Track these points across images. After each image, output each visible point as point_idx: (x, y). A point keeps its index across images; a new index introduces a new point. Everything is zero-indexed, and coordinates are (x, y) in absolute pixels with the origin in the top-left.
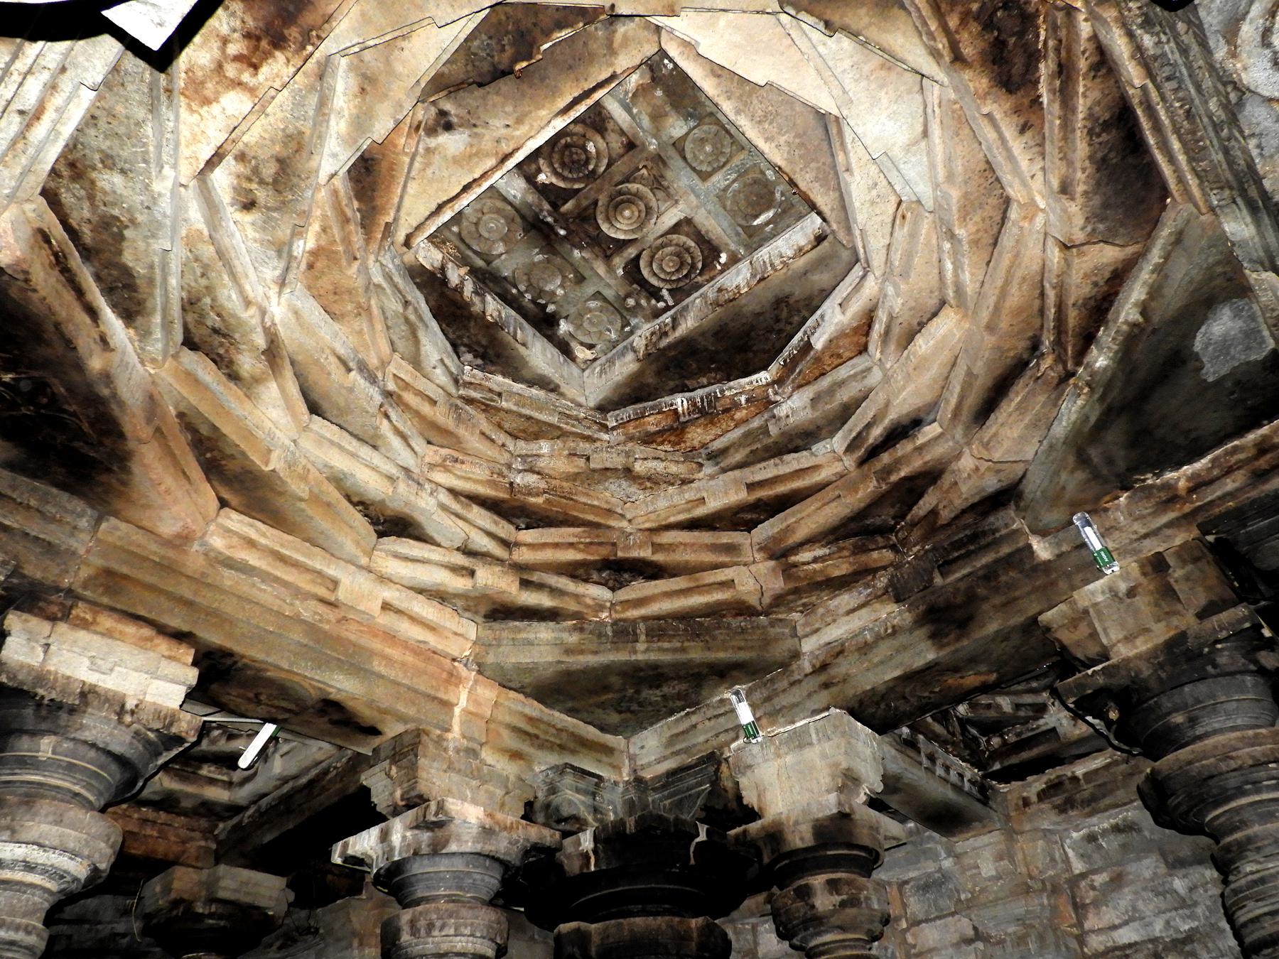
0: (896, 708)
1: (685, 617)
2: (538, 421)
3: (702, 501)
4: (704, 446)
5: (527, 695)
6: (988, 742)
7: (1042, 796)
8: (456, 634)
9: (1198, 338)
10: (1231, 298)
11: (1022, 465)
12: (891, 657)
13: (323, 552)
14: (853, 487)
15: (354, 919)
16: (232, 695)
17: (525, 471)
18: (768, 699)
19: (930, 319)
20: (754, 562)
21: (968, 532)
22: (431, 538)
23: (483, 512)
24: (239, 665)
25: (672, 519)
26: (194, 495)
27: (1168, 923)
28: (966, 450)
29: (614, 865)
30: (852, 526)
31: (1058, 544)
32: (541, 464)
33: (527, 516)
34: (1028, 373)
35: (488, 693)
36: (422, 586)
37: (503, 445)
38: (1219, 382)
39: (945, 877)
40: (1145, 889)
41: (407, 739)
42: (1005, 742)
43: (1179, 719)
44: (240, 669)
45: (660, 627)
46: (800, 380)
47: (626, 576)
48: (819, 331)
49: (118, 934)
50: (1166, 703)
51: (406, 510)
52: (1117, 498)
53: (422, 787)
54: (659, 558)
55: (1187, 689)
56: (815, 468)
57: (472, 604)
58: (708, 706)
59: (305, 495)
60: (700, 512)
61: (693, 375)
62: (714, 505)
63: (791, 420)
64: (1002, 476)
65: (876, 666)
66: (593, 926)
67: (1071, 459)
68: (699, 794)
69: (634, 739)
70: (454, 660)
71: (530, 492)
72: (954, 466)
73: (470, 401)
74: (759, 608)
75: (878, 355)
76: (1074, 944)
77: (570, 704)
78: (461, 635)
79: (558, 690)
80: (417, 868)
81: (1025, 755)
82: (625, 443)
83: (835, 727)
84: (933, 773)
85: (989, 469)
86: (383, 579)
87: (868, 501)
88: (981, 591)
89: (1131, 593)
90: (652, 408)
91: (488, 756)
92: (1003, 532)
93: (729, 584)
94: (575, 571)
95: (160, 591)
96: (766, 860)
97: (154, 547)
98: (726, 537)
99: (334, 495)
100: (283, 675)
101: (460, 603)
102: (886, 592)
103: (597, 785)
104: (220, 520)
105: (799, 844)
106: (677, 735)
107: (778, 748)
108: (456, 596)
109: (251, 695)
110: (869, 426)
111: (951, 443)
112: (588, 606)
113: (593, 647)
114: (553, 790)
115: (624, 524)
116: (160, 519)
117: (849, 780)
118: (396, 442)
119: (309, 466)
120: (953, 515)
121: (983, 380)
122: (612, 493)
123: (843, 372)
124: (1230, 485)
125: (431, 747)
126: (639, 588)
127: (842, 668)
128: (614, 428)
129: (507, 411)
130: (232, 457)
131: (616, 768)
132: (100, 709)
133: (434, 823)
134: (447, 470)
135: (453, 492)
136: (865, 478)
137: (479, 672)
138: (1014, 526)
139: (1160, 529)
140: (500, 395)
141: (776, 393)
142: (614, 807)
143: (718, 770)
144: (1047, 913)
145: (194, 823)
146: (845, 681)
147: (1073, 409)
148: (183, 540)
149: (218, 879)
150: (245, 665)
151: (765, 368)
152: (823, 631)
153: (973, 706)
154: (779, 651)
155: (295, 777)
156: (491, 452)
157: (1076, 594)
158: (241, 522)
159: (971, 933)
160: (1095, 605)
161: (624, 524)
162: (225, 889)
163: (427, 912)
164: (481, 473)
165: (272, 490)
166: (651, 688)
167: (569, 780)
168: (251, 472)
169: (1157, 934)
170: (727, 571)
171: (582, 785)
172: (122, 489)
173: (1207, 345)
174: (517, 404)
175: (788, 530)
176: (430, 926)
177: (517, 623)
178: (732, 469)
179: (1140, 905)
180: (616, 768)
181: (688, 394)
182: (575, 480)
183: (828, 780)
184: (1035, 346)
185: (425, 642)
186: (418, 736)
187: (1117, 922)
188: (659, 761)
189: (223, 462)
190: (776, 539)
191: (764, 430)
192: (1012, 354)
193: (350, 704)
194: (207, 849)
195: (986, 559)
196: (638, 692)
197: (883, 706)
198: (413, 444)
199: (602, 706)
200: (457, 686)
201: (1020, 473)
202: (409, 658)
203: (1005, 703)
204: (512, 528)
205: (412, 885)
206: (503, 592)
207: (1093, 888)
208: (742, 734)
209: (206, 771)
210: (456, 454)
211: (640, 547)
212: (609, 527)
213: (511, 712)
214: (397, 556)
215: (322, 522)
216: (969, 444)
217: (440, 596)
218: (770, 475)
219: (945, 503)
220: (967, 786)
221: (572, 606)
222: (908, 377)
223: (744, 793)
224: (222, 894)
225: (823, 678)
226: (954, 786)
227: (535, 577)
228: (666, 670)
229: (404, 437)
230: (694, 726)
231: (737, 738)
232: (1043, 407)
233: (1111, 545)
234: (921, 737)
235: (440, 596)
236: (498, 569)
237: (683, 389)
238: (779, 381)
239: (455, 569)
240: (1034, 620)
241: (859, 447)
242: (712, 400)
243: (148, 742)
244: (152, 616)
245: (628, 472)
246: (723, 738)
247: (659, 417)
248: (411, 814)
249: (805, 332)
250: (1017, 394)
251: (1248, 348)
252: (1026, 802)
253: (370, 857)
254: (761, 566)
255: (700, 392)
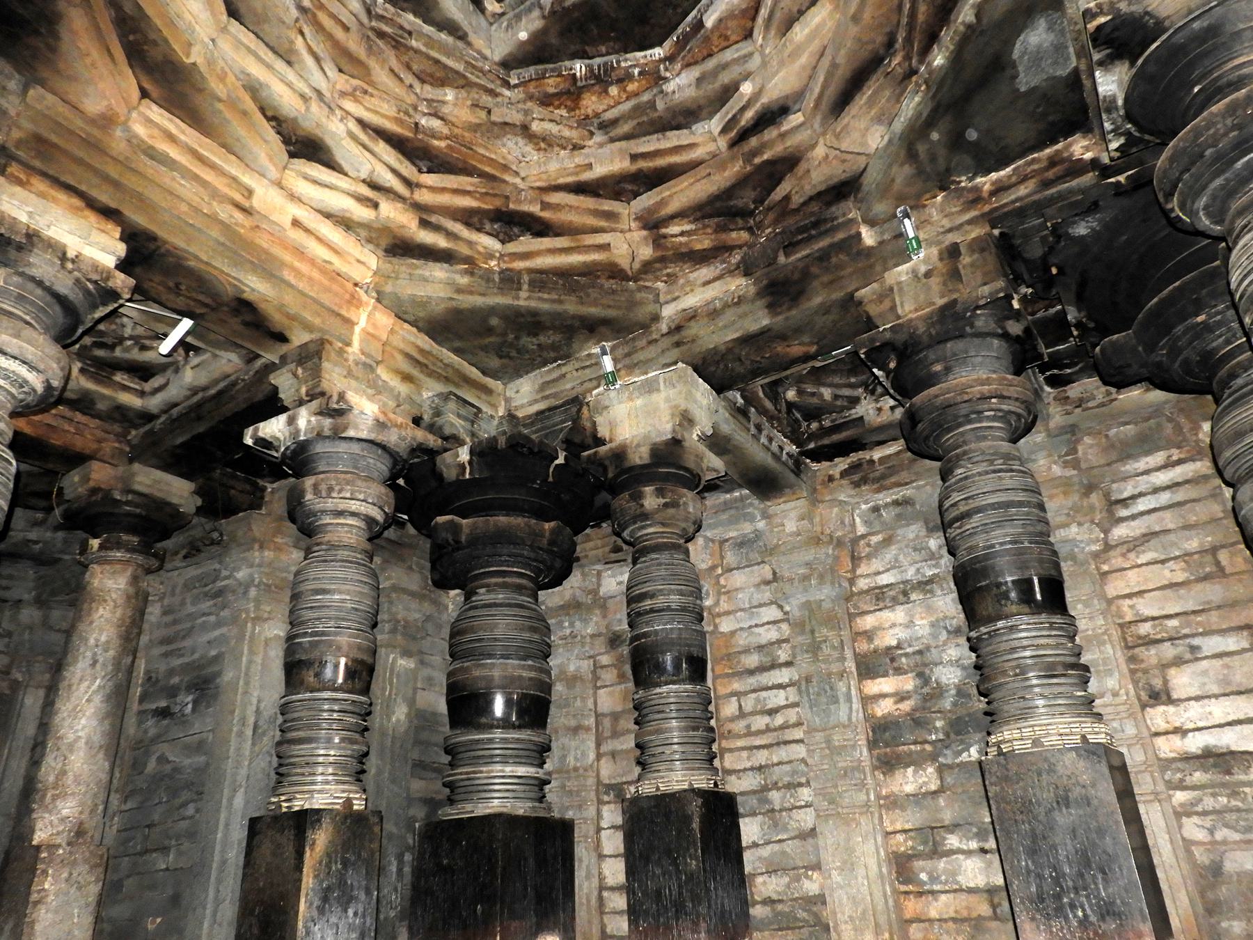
0: (733, 370)
1: (564, 274)
2: (445, 67)
3: (590, 166)
4: (597, 115)
5: (419, 330)
6: (808, 426)
7: (844, 474)
8: (358, 261)
9: (1017, 46)
10: (1047, 9)
11: (864, 158)
12: (734, 322)
13: (238, 161)
14: (722, 166)
15: (254, 527)
16: (155, 283)
17: (430, 114)
18: (628, 355)
19: (809, 8)
20: (630, 230)
21: (813, 219)
22: (340, 166)
23: (388, 148)
24: (163, 250)
25: (561, 181)
26: (118, 77)
27: (918, 569)
28: (821, 141)
29: (486, 474)
30: (718, 204)
31: (882, 233)
32: (446, 110)
33: (430, 160)
34: (881, 70)
35: (385, 320)
36: (329, 210)
37: (411, 86)
38: (1032, 91)
39: (758, 535)
40: (907, 546)
41: (312, 347)
42: (821, 427)
43: (938, 368)
44: (163, 255)
45: (541, 280)
46: (689, 59)
47: (516, 230)
48: (711, 9)
49: (29, 541)
50: (932, 356)
51: (318, 132)
52: (935, 197)
53: (325, 385)
54: (546, 215)
55: (949, 345)
56: (692, 146)
57: (374, 235)
58: (577, 359)
59: (223, 95)
60: (587, 176)
61: (594, 42)
62: (599, 171)
63: (677, 96)
64: (846, 166)
65: (721, 329)
66: (464, 521)
67: (903, 153)
68: (562, 430)
69: (511, 385)
70: (356, 285)
71: (434, 135)
72: (809, 155)
73: (381, 35)
74: (630, 273)
75: (760, 41)
76: (846, 584)
77: (457, 344)
78: (363, 263)
79: (448, 327)
80: (319, 448)
81: (836, 438)
82: (524, 102)
83: (680, 377)
84: (758, 440)
85: (836, 157)
86: (293, 197)
87: (733, 181)
88: (815, 270)
89: (928, 275)
90: (553, 70)
91: (383, 373)
92: (840, 220)
93: (605, 247)
94: (469, 218)
95: (89, 167)
96: (610, 475)
97: (80, 123)
98: (608, 205)
99: (250, 105)
100: (203, 267)
101: (364, 233)
102: (738, 267)
103: (476, 415)
104: (141, 109)
105: (638, 462)
106: (548, 382)
107: (631, 393)
108: (361, 225)
109: (171, 284)
110: (743, 109)
111: (809, 132)
112: (480, 253)
113: (482, 290)
114: (438, 413)
115: (518, 181)
116: (86, 95)
117: (687, 420)
118: (309, 61)
119: (227, 69)
120: (802, 200)
121: (843, 73)
122: (512, 149)
123: (729, 55)
124: (1022, 191)
125: (333, 354)
126: (526, 243)
127: (694, 329)
128: (516, 86)
129: (416, 51)
130: (155, 43)
131: (494, 406)
132: (46, 252)
133: (335, 410)
134: (356, 100)
135: (360, 122)
136: (733, 158)
137: (378, 300)
138: (850, 216)
139: (962, 225)
140: (410, 33)
141: (666, 69)
142: (489, 429)
143: (579, 411)
144: (830, 561)
145: (107, 426)
146: (693, 341)
147: (912, 104)
148: (107, 121)
149: (133, 475)
150: (168, 251)
151: (660, 44)
152: (681, 299)
153: (800, 392)
154: (642, 313)
155: (205, 389)
156: (399, 90)
157: (886, 275)
158: (161, 115)
159: (770, 577)
160: (899, 283)
161: (518, 181)
162: (140, 483)
163: (328, 479)
164: (388, 109)
165: (193, 86)
166: (529, 335)
167: (452, 405)
168: (172, 63)
169: (909, 578)
170: (605, 235)
171: (463, 412)
172: (50, 56)
173: (1024, 53)
174: (426, 45)
175: (662, 203)
176: (330, 489)
177: (415, 261)
178: (619, 139)
179: (901, 557)
180: (494, 406)
181: (587, 61)
182: (475, 131)
183: (668, 418)
184: (890, 43)
185: (330, 263)
186: (322, 344)
187: (881, 569)
188: (531, 404)
189: (145, 47)
190: (650, 211)
191: (652, 105)
192: (870, 47)
193: (262, 306)
194: (121, 451)
195: (824, 243)
196: (517, 338)
197: (722, 366)
198: (326, 69)
199: (485, 349)
200: (358, 308)
201: (863, 166)
202: (316, 274)
203: (827, 393)
204: (414, 170)
205: (314, 461)
206: (403, 227)
207: (869, 545)
208: (603, 382)
209: (119, 377)
210: (366, 87)
211: (530, 202)
212: (504, 181)
213: (404, 339)
214: (306, 178)
215: (238, 129)
216: (824, 134)
217: (345, 223)
218: (652, 149)
219: (797, 189)
220: (784, 457)
221: (464, 250)
222: (782, 63)
223: (599, 429)
224: (137, 487)
225: (676, 338)
226: (774, 454)
227: (434, 219)
228: (543, 319)
229: (317, 59)
230: (564, 376)
231: (598, 386)
232: (888, 101)
233: (922, 236)
234: (753, 410)
235: (345, 223)
236: (400, 205)
237: (583, 55)
238: (670, 59)
239: (361, 199)
240: (851, 296)
241: (731, 129)
242: (608, 69)
243: (87, 292)
244: (83, 188)
245: (525, 130)
246: (588, 385)
247: (559, 79)
248: (315, 404)
249: (699, 11)
250: (869, 88)
251: (1055, 63)
252: (831, 478)
253: (278, 439)
254: (635, 234)
255: (598, 60)
